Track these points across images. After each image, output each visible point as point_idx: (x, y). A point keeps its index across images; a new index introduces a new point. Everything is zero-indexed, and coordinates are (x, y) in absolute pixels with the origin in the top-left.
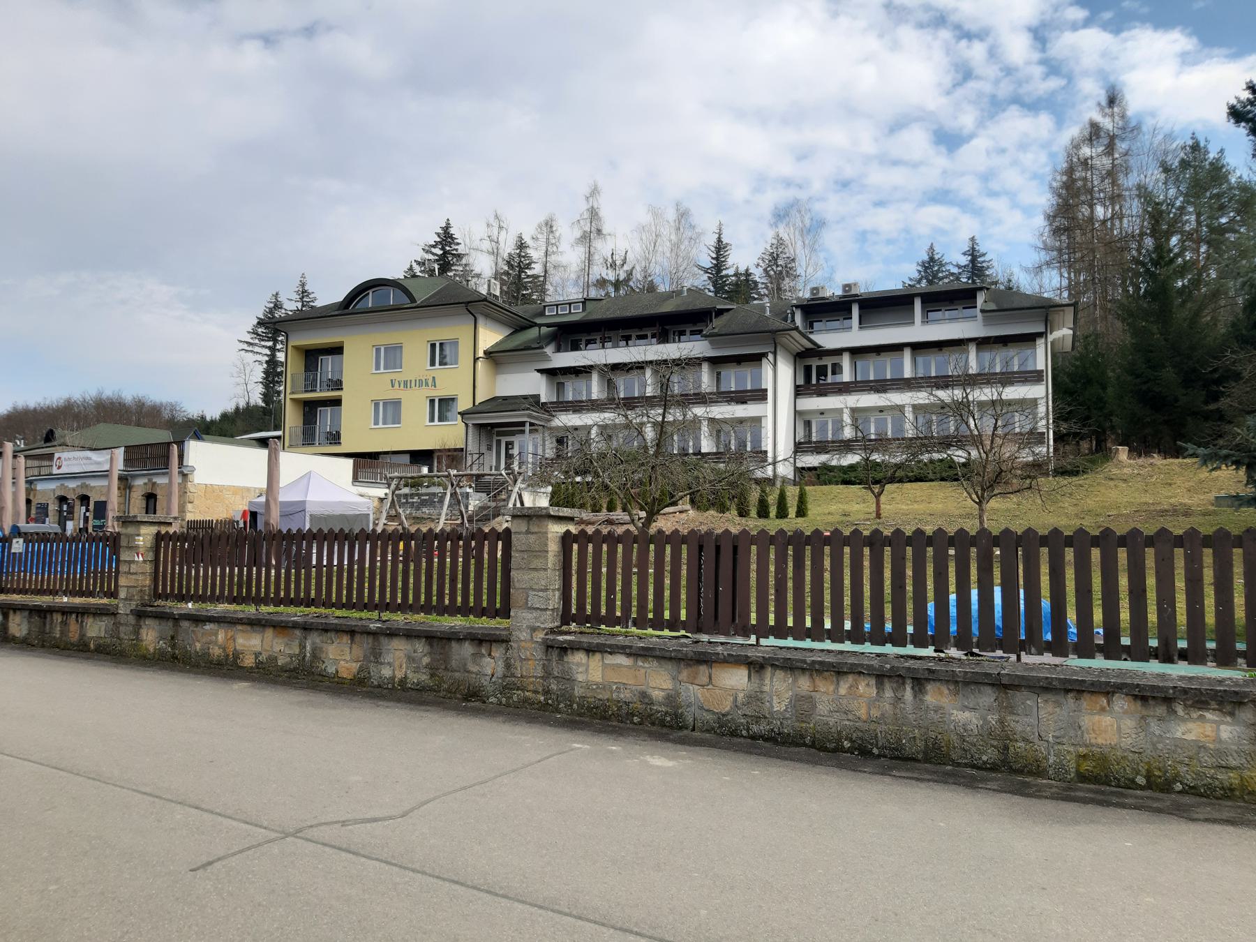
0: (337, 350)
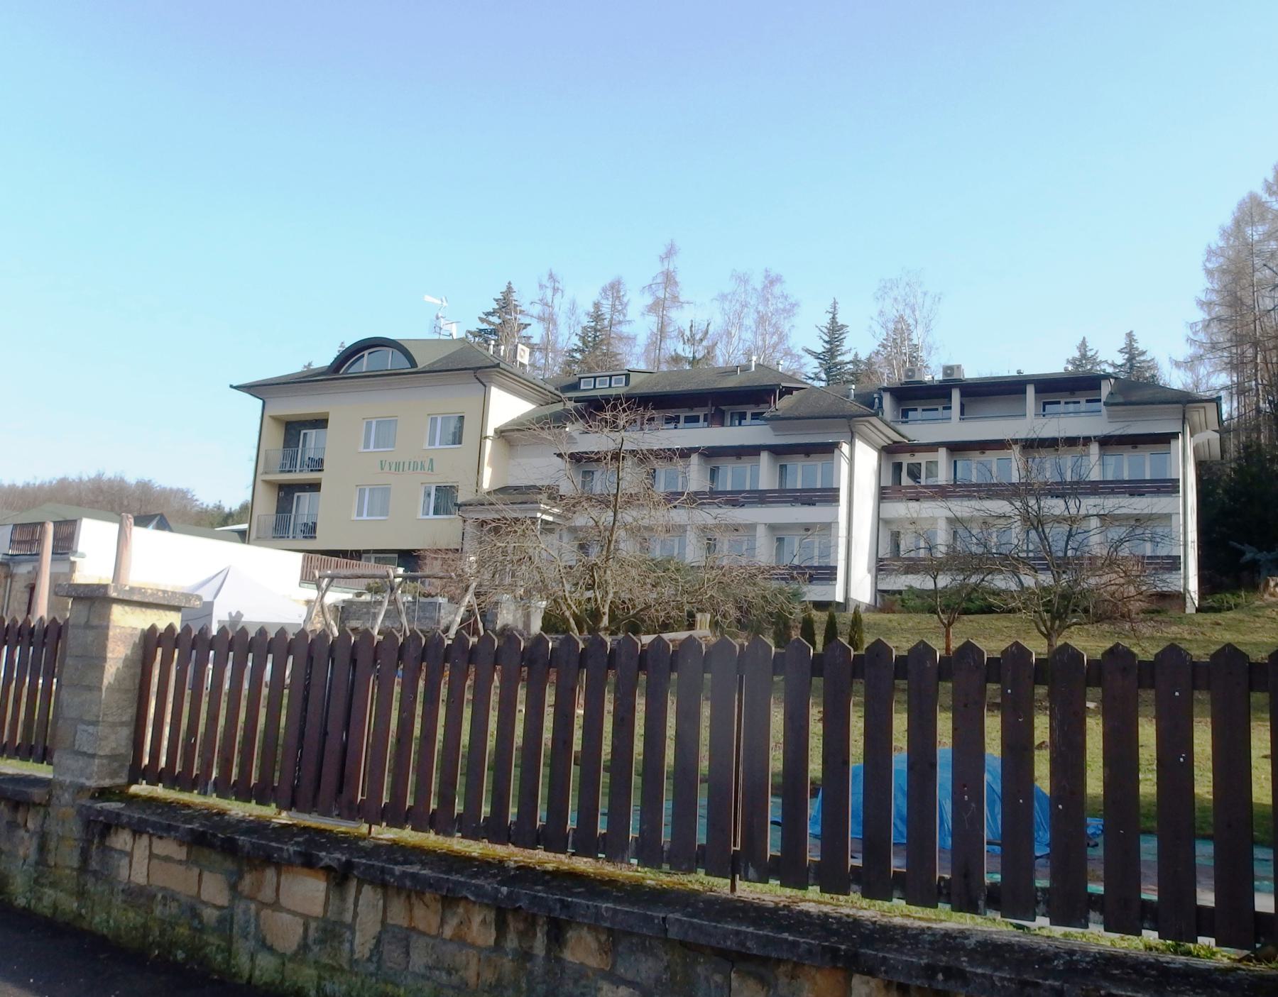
0: (320, 423)
